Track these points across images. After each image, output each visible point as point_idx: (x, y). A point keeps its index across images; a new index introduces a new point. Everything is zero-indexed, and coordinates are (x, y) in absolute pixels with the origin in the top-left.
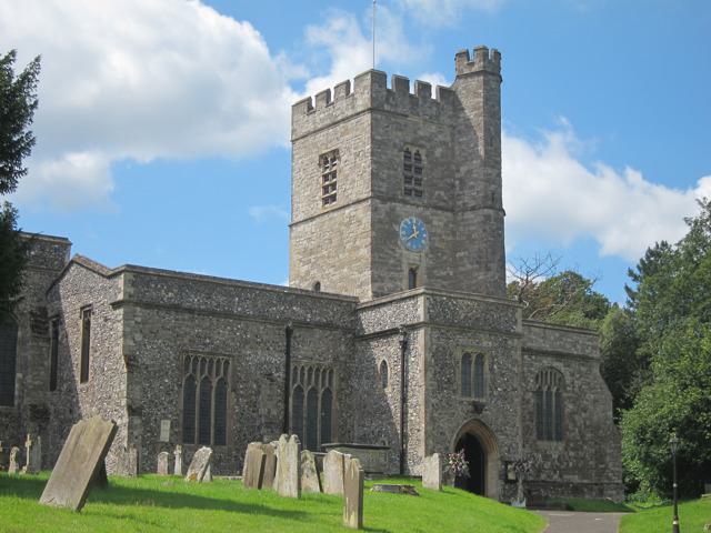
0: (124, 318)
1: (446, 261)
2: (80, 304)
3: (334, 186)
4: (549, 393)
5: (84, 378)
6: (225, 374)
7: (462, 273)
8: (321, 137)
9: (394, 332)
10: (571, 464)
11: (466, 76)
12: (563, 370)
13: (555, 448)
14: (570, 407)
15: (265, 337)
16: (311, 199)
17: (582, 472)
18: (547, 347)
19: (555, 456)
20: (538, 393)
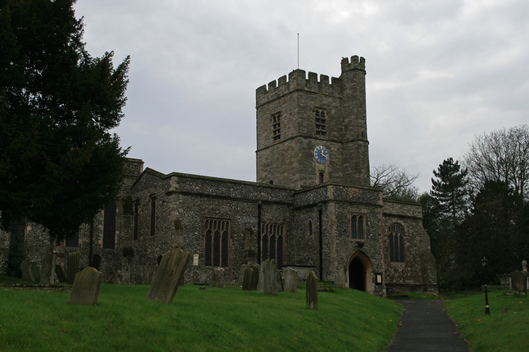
1: (338, 169)
4: (396, 237)
8: (271, 105)
9: (315, 205)
10: (409, 274)
12: (403, 224)
13: (400, 266)
18: (394, 212)
19: (400, 270)
20: (390, 237)
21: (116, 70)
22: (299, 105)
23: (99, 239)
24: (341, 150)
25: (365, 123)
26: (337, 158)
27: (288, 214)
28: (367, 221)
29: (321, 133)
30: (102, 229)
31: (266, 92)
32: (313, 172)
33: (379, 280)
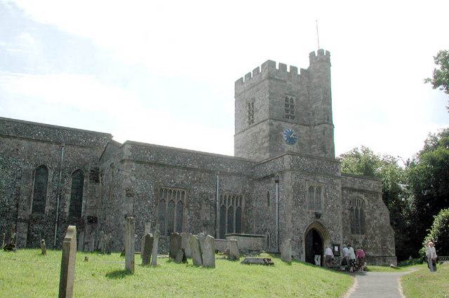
4: (357, 210)
9: (273, 175)
14: (368, 217)
17: (376, 250)
20: (351, 210)
22: (269, 91)
25: (331, 109)
26: (305, 140)
27: (248, 186)
31: (242, 83)
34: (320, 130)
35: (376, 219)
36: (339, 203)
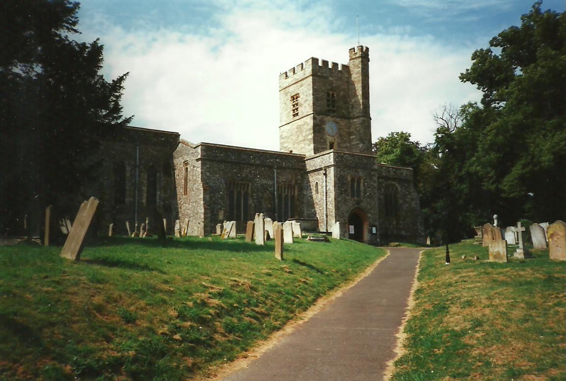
0: (201, 166)
2: (183, 161)
3: (297, 109)
5: (186, 193)
6: (248, 189)
7: (353, 145)
8: (291, 88)
9: (321, 169)
11: (354, 59)
14: (401, 201)
15: (264, 173)
16: (288, 116)
21: (548, 223)
23: (143, 199)
24: (348, 125)
26: (344, 131)
28: (364, 182)
29: (331, 111)
30: (146, 190)
32: (325, 141)
33: (374, 230)
34: (358, 123)
35: (407, 203)
36: (376, 191)
